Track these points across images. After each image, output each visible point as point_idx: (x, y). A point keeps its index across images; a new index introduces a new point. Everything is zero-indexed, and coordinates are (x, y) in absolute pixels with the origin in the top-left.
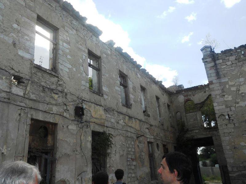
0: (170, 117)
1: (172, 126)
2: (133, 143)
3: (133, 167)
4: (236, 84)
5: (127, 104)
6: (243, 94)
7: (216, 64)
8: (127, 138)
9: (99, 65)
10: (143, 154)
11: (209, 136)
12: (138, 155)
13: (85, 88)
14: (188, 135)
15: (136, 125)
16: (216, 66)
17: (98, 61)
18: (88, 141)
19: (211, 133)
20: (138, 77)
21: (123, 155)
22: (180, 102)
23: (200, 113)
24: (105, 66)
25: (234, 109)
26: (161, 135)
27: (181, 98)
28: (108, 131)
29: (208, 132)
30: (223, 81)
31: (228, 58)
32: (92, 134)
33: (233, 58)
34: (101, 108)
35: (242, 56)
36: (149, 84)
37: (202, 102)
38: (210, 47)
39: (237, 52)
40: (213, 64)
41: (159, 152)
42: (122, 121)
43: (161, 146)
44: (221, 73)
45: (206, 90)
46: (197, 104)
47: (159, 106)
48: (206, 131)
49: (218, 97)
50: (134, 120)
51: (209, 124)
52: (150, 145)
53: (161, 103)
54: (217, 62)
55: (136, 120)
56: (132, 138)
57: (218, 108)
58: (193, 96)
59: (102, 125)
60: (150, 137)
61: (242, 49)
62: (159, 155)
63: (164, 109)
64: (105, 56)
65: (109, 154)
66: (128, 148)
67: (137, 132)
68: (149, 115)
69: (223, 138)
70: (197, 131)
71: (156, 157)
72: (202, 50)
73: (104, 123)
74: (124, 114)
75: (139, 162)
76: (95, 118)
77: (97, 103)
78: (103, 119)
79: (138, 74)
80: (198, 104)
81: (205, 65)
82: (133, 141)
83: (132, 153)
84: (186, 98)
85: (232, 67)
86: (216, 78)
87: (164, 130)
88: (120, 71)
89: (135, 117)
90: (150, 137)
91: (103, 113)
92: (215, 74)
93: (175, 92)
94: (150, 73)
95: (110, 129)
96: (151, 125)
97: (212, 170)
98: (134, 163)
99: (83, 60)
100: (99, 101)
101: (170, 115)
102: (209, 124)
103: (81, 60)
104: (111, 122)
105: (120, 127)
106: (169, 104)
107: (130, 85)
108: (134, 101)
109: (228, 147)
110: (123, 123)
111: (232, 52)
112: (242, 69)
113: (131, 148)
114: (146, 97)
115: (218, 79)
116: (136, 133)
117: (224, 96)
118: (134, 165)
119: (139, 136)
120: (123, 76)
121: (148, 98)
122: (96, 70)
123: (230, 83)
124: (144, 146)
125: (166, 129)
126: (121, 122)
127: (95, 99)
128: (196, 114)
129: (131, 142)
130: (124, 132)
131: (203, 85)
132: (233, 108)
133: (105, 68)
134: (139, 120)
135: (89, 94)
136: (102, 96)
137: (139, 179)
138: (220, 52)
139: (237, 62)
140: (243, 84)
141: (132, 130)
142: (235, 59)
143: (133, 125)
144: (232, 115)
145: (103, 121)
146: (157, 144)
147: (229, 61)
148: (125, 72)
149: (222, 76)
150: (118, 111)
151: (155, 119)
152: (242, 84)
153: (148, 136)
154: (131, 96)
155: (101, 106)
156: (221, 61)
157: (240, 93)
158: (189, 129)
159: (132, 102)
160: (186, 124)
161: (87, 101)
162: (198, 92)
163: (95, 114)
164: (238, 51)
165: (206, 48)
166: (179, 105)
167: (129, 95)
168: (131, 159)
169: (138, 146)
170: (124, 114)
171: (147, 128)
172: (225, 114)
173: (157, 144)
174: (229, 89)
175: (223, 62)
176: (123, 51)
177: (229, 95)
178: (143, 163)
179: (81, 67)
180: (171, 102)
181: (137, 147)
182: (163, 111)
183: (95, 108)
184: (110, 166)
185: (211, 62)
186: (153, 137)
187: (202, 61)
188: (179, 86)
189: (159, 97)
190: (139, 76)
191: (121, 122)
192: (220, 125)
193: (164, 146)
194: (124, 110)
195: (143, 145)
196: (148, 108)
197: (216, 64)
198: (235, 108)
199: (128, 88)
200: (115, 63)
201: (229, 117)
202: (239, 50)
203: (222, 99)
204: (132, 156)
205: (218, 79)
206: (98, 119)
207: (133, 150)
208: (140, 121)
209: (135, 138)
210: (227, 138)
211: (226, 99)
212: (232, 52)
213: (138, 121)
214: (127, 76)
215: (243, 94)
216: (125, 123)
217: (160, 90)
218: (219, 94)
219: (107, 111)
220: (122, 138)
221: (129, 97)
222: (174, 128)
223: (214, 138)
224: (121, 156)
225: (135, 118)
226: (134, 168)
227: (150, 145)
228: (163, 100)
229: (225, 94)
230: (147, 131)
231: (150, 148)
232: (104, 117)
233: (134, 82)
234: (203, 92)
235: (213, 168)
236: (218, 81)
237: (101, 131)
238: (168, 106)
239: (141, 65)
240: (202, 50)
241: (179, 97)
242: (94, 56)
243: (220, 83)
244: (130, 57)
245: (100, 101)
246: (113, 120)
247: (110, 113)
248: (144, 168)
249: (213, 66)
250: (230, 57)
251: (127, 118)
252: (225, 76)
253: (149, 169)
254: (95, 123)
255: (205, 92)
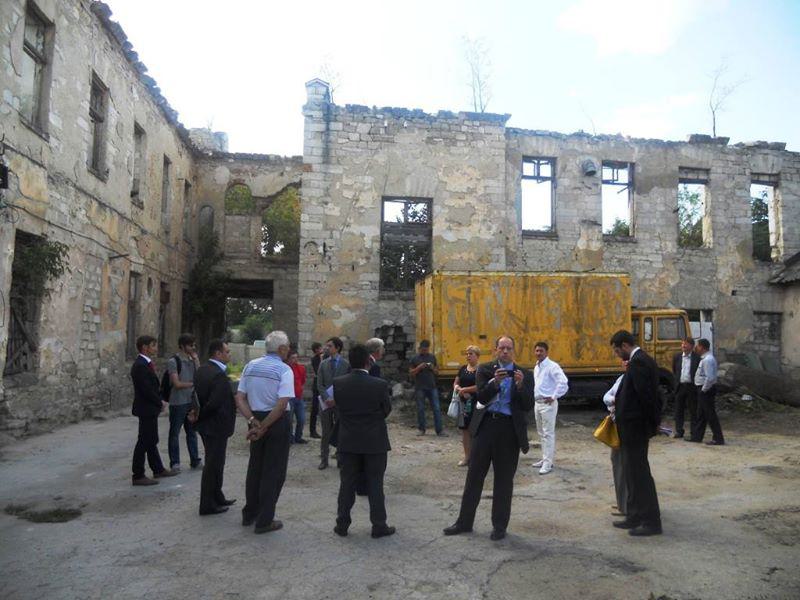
0: (186, 215)
1: (187, 241)
2: (99, 271)
3: (93, 328)
4: (355, 186)
5: (97, 167)
6: (362, 211)
7: (328, 129)
8: (88, 257)
9: (47, 47)
10: (117, 299)
11: (269, 277)
12: (106, 302)
13: (10, 113)
14: (221, 268)
15: (109, 224)
16: (328, 135)
17: (43, 34)
18: (6, 254)
19: (273, 271)
20: (133, 99)
21: (76, 297)
22: (218, 182)
23: (259, 220)
24: (62, 54)
25: (338, 237)
26: (161, 258)
27: (223, 174)
28: (56, 237)
29: (266, 269)
30: (332, 171)
31: (355, 124)
32: (17, 238)
33: (364, 128)
34: (42, 173)
35: (382, 131)
36: (154, 120)
37: (269, 197)
38: (326, 86)
39: (376, 117)
40: (322, 127)
41: (150, 300)
42: (83, 212)
43: (156, 286)
44: (333, 153)
45: (284, 170)
46: (256, 197)
47: (166, 182)
48: (265, 266)
49: (314, 203)
50: (108, 213)
51: (270, 249)
52: (133, 280)
53: (172, 177)
54: (333, 126)
55: (115, 214)
56: (98, 257)
57: (309, 226)
58: (253, 175)
59: (39, 218)
60: (137, 263)
61: (388, 115)
62: (148, 307)
63: (175, 194)
64: (66, 22)
65: (48, 292)
66: (88, 281)
67: (112, 243)
68: (142, 203)
69: (302, 291)
70: (243, 262)
71: (142, 311)
72: (308, 85)
73: (44, 213)
74: (90, 196)
75: (107, 316)
76: (27, 198)
77: (35, 159)
78: (44, 202)
79: (134, 90)
80: (260, 198)
81: (306, 122)
82: (101, 266)
83: (94, 295)
84: (234, 177)
85: (358, 147)
86: (321, 160)
87: (168, 246)
88: (94, 74)
89: (112, 206)
90: (137, 261)
91: (45, 187)
92: (320, 152)
93: (211, 154)
94: (162, 93)
95: (55, 230)
96: (144, 232)
97: (246, 349)
98: (97, 319)
99: (13, 28)
100: (38, 152)
101: (187, 209)
102: (270, 249)
103: (7, 29)
104: (60, 211)
105: (77, 227)
106: (189, 180)
107: (112, 117)
108: (114, 163)
109: (308, 311)
110: (85, 218)
111: (366, 115)
112: (376, 157)
113: (93, 282)
114: (141, 156)
115: (324, 163)
116: (108, 246)
117: (326, 203)
118: (96, 324)
119: (116, 255)
120: (99, 90)
121: (147, 157)
122: (35, 60)
123: (346, 181)
124: (120, 281)
125: (173, 245)
126: (81, 215)
127: (31, 144)
128: (249, 222)
129: (96, 269)
130: (84, 241)
131: (282, 156)
132: (336, 234)
133: (61, 58)
134: (119, 214)
135: (17, 129)
136: (47, 140)
137: (101, 355)
138: (344, 106)
139: (370, 139)
140: (369, 190)
141: (103, 240)
142: (367, 131)
143: (105, 226)
144: (331, 247)
145: (41, 207)
146: (150, 279)
147: (355, 132)
148: (104, 81)
149: (334, 160)
150: (77, 184)
151: (153, 217)
152: (366, 188)
153: (133, 258)
154: (111, 149)
155: (41, 166)
156: (339, 126)
157: (358, 205)
158: (226, 254)
159: (110, 164)
160: (221, 240)
161: (12, 150)
162: (267, 170)
163: (28, 186)
164: (378, 116)
165: (317, 85)
166: (214, 190)
167: (105, 144)
168: (92, 308)
169: (110, 280)
170: (90, 196)
171: (135, 238)
172: (320, 242)
173: (150, 279)
174: (340, 192)
175: (343, 130)
176: (112, 18)
177: (337, 204)
178: (114, 323)
179: (4, 46)
180: (195, 178)
181: (107, 281)
182: (173, 197)
183: (28, 169)
184: (46, 321)
185: (319, 122)
186: (142, 261)
187: (301, 110)
188: (216, 134)
189: (172, 160)
190: (136, 96)
191: (81, 215)
192: (304, 264)
193: (163, 285)
194: (90, 182)
195: (121, 278)
196: (141, 186)
197: (328, 129)
198: (341, 234)
199: (106, 126)
200: (87, 50)
201: (325, 251)
202: (381, 116)
203: (320, 210)
204: (94, 303)
205: (324, 163)
206: (32, 199)
207: (98, 288)
208: (122, 216)
209: (106, 258)
210: (311, 292)
211: (329, 213)
212: (366, 115)
213: (117, 218)
214: (107, 90)
215: (362, 211)
216: (89, 218)
217: (175, 140)
218: (318, 198)
219: (53, 183)
220: (78, 256)
221: (104, 148)
222: (190, 244)
223: (276, 285)
224: (73, 299)
225: (111, 208)
226: (94, 330)
227: (133, 280)
228: (178, 169)
229: (328, 199)
230: (133, 244)
231: (133, 287)
232: (46, 198)
233: (124, 108)
234: (276, 174)
235: (250, 346)
236: (322, 168)
237: (37, 232)
238: (187, 185)
239: (156, 79)
240: (308, 85)
241: (217, 169)
242: (37, 16)
243: (325, 173)
244: (124, 37)
245: (41, 153)
246: (64, 208)
247: (60, 188)
248: (115, 332)
249: (322, 132)
250: (360, 124)
251: (95, 205)
252: (339, 163)
253: (125, 335)
254: (24, 209)
255: (282, 174)
